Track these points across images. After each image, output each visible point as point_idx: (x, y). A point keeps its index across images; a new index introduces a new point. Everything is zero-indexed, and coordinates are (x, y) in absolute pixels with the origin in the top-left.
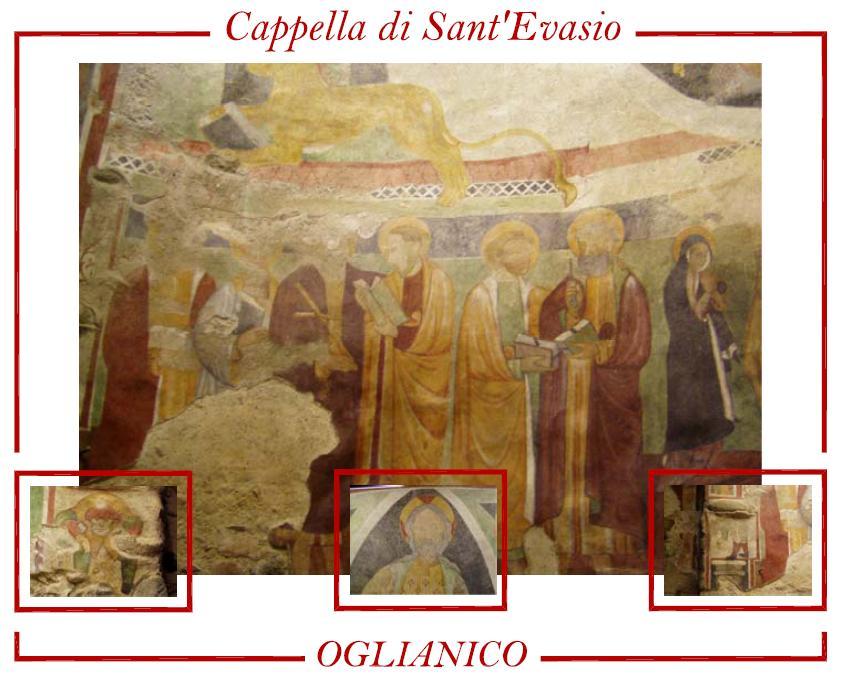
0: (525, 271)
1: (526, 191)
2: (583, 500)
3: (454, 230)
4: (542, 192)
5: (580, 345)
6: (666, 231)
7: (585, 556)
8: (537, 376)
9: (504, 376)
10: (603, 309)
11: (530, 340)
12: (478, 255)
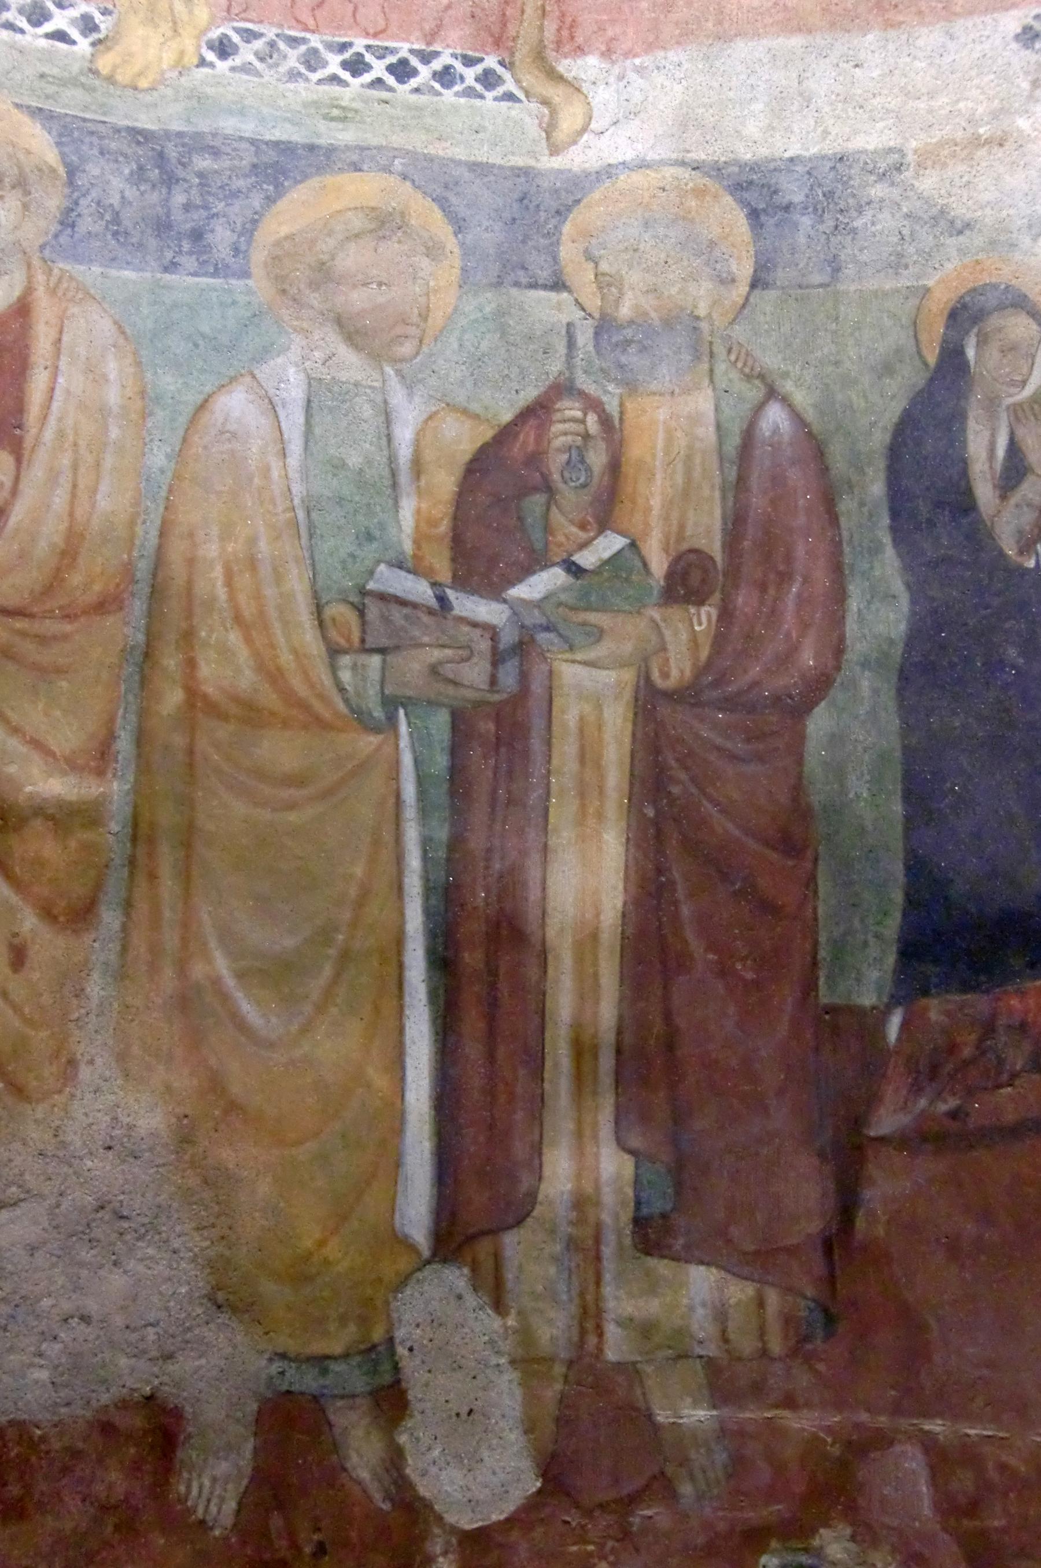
0: (406, 349)
1: (414, 82)
2: (613, 1166)
3: (155, 174)
4: (469, 92)
5: (592, 617)
6: (897, 263)
7: (619, 1366)
8: (440, 722)
9: (327, 715)
10: (673, 505)
11: (420, 590)
12: (246, 274)
